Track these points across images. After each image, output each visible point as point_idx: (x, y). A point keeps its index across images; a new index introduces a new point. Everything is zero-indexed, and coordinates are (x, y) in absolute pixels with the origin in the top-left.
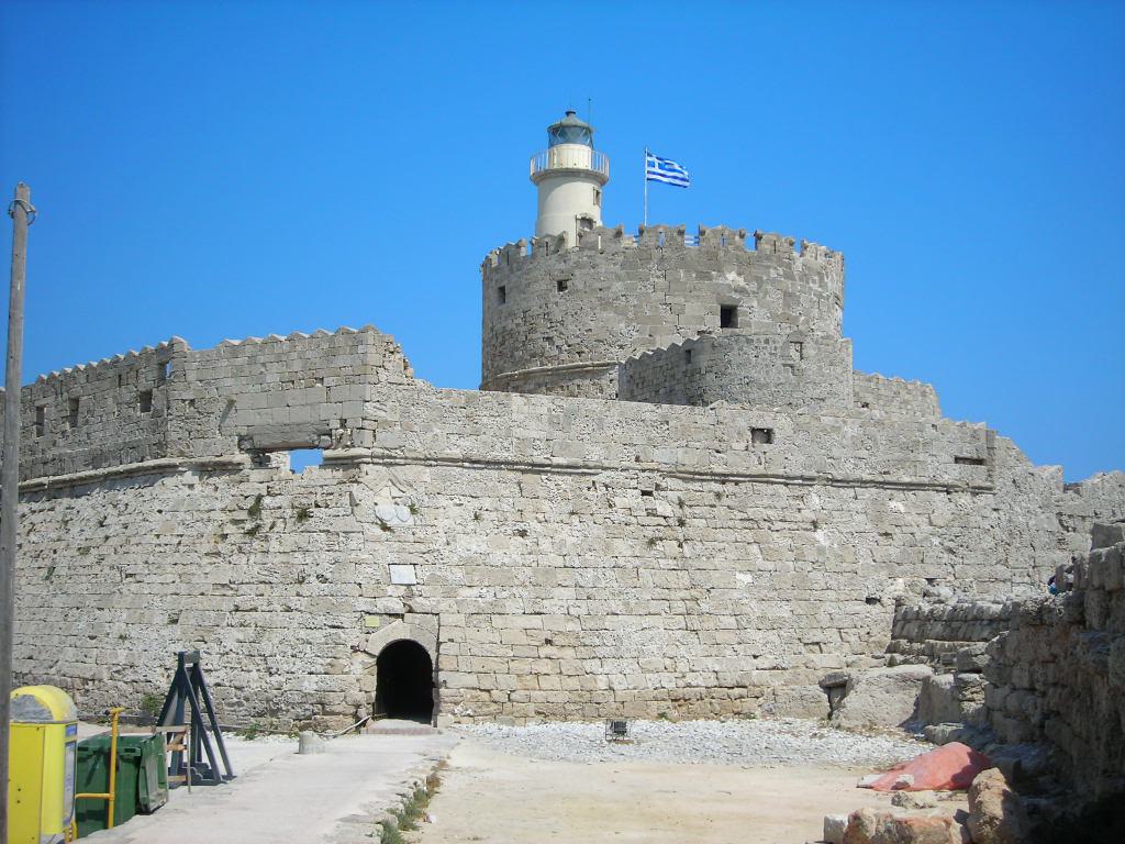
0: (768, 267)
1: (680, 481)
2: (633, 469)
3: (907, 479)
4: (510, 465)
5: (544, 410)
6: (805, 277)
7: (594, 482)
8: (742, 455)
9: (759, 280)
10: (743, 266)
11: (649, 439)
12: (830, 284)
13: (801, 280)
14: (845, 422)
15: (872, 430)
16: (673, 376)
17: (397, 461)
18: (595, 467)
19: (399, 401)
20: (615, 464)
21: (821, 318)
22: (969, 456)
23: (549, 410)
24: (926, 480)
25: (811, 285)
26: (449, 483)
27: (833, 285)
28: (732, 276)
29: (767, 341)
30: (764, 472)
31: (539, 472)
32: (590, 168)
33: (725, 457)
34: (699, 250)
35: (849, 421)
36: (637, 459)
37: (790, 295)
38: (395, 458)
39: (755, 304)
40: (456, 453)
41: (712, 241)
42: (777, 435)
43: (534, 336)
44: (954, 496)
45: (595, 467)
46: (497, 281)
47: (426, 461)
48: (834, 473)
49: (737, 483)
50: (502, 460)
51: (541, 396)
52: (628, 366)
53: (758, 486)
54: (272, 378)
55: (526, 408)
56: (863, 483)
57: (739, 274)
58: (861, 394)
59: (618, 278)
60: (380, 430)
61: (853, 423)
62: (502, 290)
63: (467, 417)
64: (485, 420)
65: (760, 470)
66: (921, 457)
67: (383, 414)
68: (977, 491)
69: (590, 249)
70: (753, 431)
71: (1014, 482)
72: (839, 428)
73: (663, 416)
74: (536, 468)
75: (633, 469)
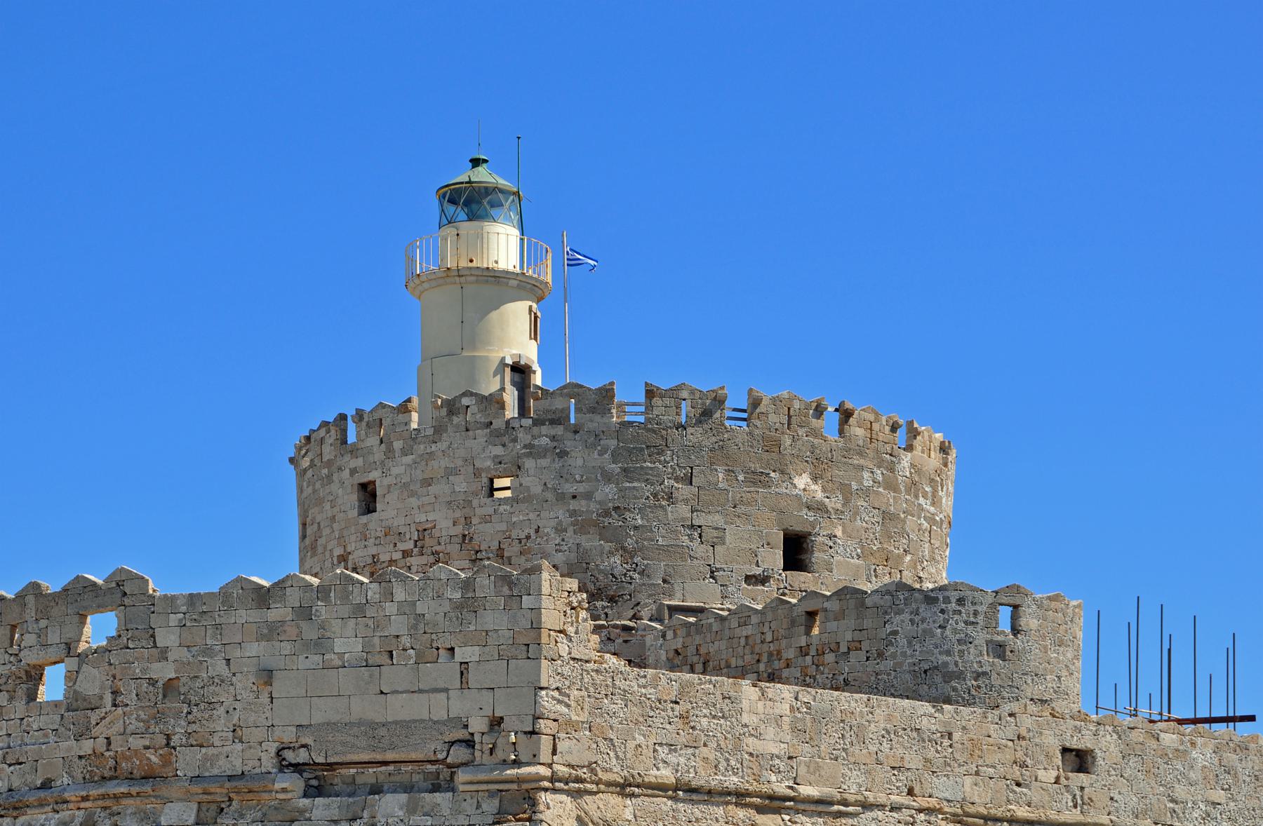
0: (862, 468)
2: (908, 808)
4: (740, 797)
5: (785, 708)
9: (845, 490)
10: (819, 467)
11: (927, 760)
13: (908, 491)
14: (1193, 744)
15: (1231, 758)
19: (587, 689)
20: (882, 798)
23: (792, 708)
25: (922, 501)
28: (802, 481)
29: (961, 601)
31: (777, 811)
33: (1029, 793)
35: (1199, 741)
40: (666, 775)
41: (773, 418)
42: (1100, 762)
46: (353, 472)
47: (624, 788)
51: (779, 685)
54: (347, 644)
55: (760, 704)
57: (815, 479)
59: (608, 478)
61: (1205, 745)
69: (553, 422)
70: (1065, 750)
73: (945, 724)
74: (773, 803)
75: (908, 808)
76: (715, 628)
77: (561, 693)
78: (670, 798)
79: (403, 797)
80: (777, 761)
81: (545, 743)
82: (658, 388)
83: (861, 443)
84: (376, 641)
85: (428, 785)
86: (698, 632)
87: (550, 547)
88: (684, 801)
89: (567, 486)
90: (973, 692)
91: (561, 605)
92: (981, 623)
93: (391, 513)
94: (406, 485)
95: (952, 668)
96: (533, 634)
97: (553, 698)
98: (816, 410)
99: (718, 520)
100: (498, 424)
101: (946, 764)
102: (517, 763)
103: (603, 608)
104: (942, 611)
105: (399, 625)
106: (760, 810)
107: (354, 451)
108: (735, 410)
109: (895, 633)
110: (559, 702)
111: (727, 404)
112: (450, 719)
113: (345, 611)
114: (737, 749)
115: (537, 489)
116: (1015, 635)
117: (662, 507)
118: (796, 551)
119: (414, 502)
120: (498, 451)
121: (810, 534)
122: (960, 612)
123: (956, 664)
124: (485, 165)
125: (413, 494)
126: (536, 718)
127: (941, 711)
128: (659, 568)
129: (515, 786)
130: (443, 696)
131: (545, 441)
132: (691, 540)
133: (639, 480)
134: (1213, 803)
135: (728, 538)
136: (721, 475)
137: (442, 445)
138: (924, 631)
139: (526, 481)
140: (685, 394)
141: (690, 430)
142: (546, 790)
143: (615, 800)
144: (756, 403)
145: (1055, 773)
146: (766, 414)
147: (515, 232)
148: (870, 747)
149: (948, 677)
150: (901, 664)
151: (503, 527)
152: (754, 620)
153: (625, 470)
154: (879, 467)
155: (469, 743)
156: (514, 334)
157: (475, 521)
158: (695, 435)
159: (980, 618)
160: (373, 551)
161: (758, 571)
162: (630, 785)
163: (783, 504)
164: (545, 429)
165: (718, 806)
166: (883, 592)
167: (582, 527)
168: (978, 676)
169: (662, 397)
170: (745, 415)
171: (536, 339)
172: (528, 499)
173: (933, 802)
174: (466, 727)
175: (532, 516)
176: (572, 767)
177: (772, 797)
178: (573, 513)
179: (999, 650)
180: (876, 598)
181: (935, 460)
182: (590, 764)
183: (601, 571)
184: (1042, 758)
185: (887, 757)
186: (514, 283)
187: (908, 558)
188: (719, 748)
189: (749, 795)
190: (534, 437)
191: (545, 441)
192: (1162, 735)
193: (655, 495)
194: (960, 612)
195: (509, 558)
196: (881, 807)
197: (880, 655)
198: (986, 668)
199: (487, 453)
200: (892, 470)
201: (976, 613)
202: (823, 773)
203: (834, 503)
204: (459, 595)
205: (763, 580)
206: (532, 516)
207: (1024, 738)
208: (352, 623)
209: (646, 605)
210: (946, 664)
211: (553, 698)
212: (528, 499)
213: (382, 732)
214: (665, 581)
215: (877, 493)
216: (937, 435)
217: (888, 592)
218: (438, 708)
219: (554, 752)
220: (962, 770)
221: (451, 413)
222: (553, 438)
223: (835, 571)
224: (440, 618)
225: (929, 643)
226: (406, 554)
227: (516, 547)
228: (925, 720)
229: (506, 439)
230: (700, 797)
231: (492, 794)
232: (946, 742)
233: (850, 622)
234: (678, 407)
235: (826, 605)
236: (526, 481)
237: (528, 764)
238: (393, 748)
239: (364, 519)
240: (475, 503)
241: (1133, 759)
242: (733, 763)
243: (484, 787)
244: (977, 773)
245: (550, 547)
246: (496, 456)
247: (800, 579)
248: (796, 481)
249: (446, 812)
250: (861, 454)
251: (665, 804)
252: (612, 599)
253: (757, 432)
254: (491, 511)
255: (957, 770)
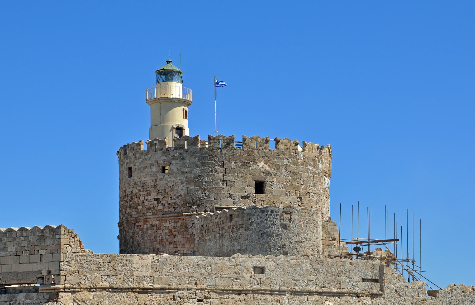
1: (217, 295)
3: (335, 290)
4: (132, 290)
6: (305, 163)
7: (174, 296)
8: (248, 281)
11: (202, 274)
12: (320, 166)
14: (302, 262)
16: (223, 228)
17: (77, 290)
18: (175, 289)
19: (77, 261)
20: (185, 286)
21: (315, 186)
22: (370, 278)
23: (152, 262)
24: (345, 291)
25: (309, 167)
26: (102, 300)
27: (323, 165)
28: (261, 164)
30: (260, 288)
31: (147, 293)
32: (181, 97)
34: (243, 150)
35: (305, 261)
36: (196, 284)
37: (296, 174)
38: (75, 288)
39: (275, 180)
40: (106, 285)
42: (267, 270)
43: (149, 198)
44: (362, 299)
45: (175, 289)
46: (127, 164)
47: (90, 290)
48: (296, 288)
49: (246, 294)
50: (129, 287)
52: (200, 220)
53: (256, 295)
54: (11, 249)
55: (140, 261)
56: (311, 293)
57: (266, 163)
58: (332, 233)
59: (197, 166)
60: (68, 275)
62: (130, 169)
63: (111, 267)
64: (120, 268)
65: (258, 287)
66: (343, 279)
67: (69, 267)
68: (373, 296)
70: (255, 268)
71: (396, 291)
72: (299, 265)
74: (144, 291)
76: (210, 219)
77: (68, 263)
78: (107, 291)
79: (25, 294)
80: (146, 278)
81: (62, 278)
82: (212, 137)
83: (283, 150)
84: (19, 248)
85: (34, 290)
86: (207, 220)
87: (179, 189)
88: (112, 292)
89: (184, 169)
90: (276, 240)
91: (68, 237)
92: (279, 218)
93: (136, 178)
94: (139, 169)
95: (269, 233)
96: (59, 246)
97: (65, 264)
98: (266, 140)
99: (232, 178)
100: (164, 149)
101: (209, 275)
102: (55, 284)
103: (195, 208)
104: (266, 215)
105: (24, 244)
106: (139, 293)
107: (127, 157)
108: (238, 142)
109: (252, 222)
110: (67, 265)
111: (235, 141)
112: (37, 271)
113: (11, 239)
114: (131, 275)
115: (175, 170)
116: (290, 222)
117: (214, 175)
118: (260, 187)
119: (142, 174)
120: (164, 158)
121: (264, 181)
122: (272, 215)
123: (271, 231)
124: (171, 63)
125: (141, 172)
126: (60, 270)
127: (207, 258)
128: (213, 195)
129: (53, 291)
130: (36, 264)
131: (178, 154)
132: (223, 185)
133: (206, 167)
134: (310, 280)
135: (236, 184)
136: (233, 164)
137: (149, 156)
138: (261, 221)
139: (172, 167)
140: (221, 138)
141: (223, 150)
142: (62, 292)
143: (86, 293)
144: (244, 140)
145: (250, 275)
146: (248, 143)
147: (180, 85)
148: (181, 271)
149: (269, 235)
150: (254, 232)
151: (166, 182)
152: (219, 217)
153: (202, 163)
154: (290, 158)
155: (42, 278)
156: (178, 117)
157: (158, 180)
158: (224, 151)
159: (278, 216)
160: (131, 189)
161: (246, 194)
162: (92, 288)
163: (254, 172)
164: (178, 151)
165: (124, 292)
166: (250, 209)
167: (189, 182)
168: (278, 235)
169: (213, 139)
170: (242, 144)
171: (186, 118)
172: (173, 173)
173: (204, 287)
174: (42, 273)
175: (174, 179)
176: (72, 284)
177: (144, 289)
178: (186, 178)
179: (284, 226)
180: (247, 211)
181: (315, 152)
182: (78, 283)
183: (195, 196)
184: (245, 270)
185: (187, 274)
186: (177, 101)
187: (303, 186)
188: (125, 275)
189: (136, 289)
190: (175, 154)
191: (178, 154)
192: (290, 260)
193: (212, 171)
194: (272, 215)
195: (167, 192)
196: (184, 289)
197: (248, 229)
198: (280, 233)
199: (161, 159)
200: (296, 158)
201: (277, 215)
202: (163, 280)
203: (273, 170)
204: (40, 235)
205: (248, 197)
206: (174, 179)
207: (238, 265)
208: (12, 243)
209: (209, 207)
210: (267, 232)
211: (65, 264)
212: (173, 173)
213: (20, 275)
214: (215, 199)
215: (290, 166)
216: (316, 145)
217: (251, 209)
218: (33, 267)
219: (65, 280)
220: (215, 276)
221: (151, 146)
222: (180, 154)
223: (273, 193)
224: (35, 241)
225: (263, 225)
226: (140, 191)
227: (170, 189)
228: (201, 262)
229: (166, 154)
230: (117, 290)
231: (47, 293)
232: (209, 268)
233: (240, 219)
234: (219, 142)
235: (234, 213)
236: (172, 167)
237: (57, 284)
238: (23, 279)
239: (129, 179)
240: (158, 175)
241: (279, 269)
242: (130, 279)
243: (45, 291)
244: (221, 277)
245: (179, 189)
246: (164, 160)
247: (261, 196)
248: (259, 164)
249: (35, 299)
250: (283, 154)
251: (105, 293)
252: (198, 205)
253: (245, 149)
254: (162, 177)
255: (213, 276)
